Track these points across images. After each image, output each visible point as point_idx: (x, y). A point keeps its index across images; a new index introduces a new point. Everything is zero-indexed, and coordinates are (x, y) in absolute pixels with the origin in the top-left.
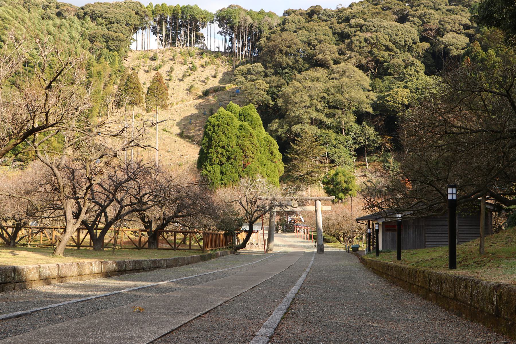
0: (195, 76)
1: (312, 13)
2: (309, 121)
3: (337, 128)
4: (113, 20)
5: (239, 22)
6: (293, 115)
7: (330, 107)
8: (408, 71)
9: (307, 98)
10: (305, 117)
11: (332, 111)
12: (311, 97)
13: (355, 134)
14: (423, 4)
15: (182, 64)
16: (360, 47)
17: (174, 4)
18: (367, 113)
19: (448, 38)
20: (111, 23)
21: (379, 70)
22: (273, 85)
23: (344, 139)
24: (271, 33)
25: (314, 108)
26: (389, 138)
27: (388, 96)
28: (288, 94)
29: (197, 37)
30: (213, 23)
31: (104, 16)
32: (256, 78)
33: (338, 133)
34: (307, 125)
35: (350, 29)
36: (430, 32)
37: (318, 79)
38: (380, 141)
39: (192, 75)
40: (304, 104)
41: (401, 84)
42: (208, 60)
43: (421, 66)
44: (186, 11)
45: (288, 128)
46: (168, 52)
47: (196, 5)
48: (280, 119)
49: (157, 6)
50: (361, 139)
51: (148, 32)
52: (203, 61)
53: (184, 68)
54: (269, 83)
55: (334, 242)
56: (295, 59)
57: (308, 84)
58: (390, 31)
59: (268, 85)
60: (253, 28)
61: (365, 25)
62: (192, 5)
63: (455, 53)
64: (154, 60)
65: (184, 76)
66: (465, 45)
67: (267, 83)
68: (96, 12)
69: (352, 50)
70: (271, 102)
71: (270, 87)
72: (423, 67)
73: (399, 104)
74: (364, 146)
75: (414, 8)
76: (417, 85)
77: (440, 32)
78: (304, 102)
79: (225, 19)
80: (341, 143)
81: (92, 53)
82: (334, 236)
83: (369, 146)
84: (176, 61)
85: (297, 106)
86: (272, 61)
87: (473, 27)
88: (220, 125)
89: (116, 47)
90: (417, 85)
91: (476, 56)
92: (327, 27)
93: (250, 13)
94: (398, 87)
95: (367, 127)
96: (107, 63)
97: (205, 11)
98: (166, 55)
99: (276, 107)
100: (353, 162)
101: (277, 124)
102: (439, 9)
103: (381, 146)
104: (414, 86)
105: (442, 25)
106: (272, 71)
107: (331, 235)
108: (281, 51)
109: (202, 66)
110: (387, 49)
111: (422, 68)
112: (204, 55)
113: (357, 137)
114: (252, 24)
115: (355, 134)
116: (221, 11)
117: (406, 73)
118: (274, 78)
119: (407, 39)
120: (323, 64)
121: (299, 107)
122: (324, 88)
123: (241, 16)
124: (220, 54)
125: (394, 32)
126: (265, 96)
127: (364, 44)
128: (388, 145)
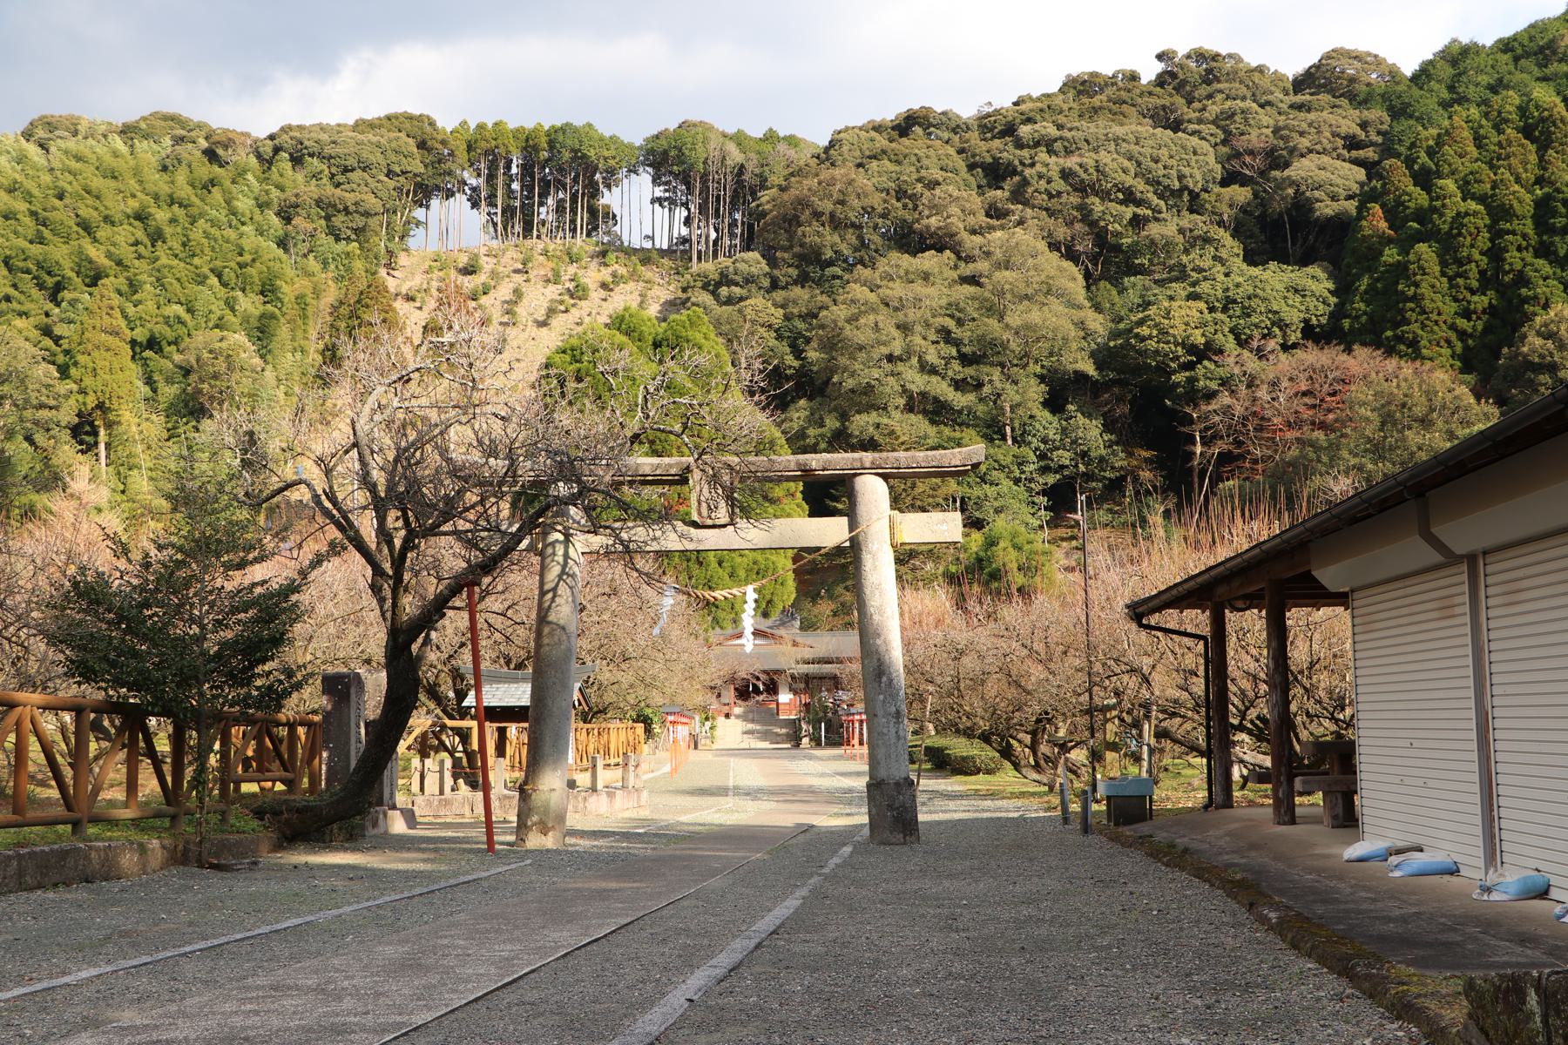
0: (584, 313)
1: (908, 124)
2: (902, 402)
3: (988, 427)
4: (351, 162)
5: (705, 162)
6: (850, 383)
7: (965, 360)
8: (1193, 258)
9: (896, 333)
10: (888, 390)
11: (970, 371)
12: (904, 328)
13: (1044, 441)
14: (1221, 91)
15: (548, 281)
16: (1051, 196)
17: (529, 124)
18: (1081, 377)
19: (1301, 169)
20: (346, 170)
21: (1106, 261)
22: (795, 311)
23: (1009, 459)
24: (792, 174)
25: (914, 361)
26: (1146, 454)
27: (1141, 323)
28: (835, 322)
29: (593, 212)
30: (636, 172)
31: (328, 150)
32: (744, 292)
33: (992, 440)
34: (897, 415)
35: (1018, 152)
36: (1248, 159)
37: (926, 277)
38: (1120, 460)
39: (573, 310)
40: (885, 350)
41: (1180, 289)
42: (622, 271)
43: (1231, 246)
44: (561, 138)
45: (838, 424)
46: (512, 253)
47: (590, 125)
48: (811, 399)
49: (481, 127)
50: (1064, 457)
51: (461, 202)
52: (605, 274)
53: (553, 291)
54: (783, 307)
55: (989, 772)
56: (861, 238)
57: (897, 290)
58: (1135, 149)
59: (782, 311)
60: (746, 177)
61: (1061, 138)
62: (578, 122)
63: (1326, 209)
64: (471, 273)
65: (551, 312)
66: (1355, 188)
67: (775, 305)
68: (306, 143)
69: (1026, 203)
70: (790, 360)
71: (787, 318)
72: (1238, 248)
73: (1176, 344)
74: (1072, 478)
75: (1196, 105)
76: (1228, 289)
77: (1276, 159)
78: (884, 344)
79: (669, 160)
80: (1002, 468)
81: (286, 250)
82: (985, 737)
83: (1088, 477)
84: (532, 274)
85: (862, 356)
86: (791, 247)
87: (1372, 144)
88: (583, 373)
89: (357, 231)
90: (1228, 289)
91: (1399, 203)
92: (952, 151)
93: (739, 139)
94: (1171, 298)
95: (1081, 420)
96: (330, 275)
97: (614, 139)
98: (503, 261)
99: (805, 375)
100: (1041, 527)
101: (804, 414)
102: (1269, 103)
103: (1123, 478)
104: (1220, 293)
105: (1282, 138)
106: (794, 272)
107: (969, 733)
108: (817, 215)
109: (604, 286)
110: (1130, 198)
111: (1236, 250)
112: (611, 256)
113: (1051, 450)
114: (742, 166)
115: (1044, 441)
116: (657, 137)
117: (1190, 267)
118: (797, 291)
119: (1186, 171)
120: (940, 242)
121: (870, 359)
122: (944, 302)
123: (712, 145)
124: (655, 255)
125: (1147, 151)
126: (773, 342)
127: (1058, 184)
128: (1146, 475)
